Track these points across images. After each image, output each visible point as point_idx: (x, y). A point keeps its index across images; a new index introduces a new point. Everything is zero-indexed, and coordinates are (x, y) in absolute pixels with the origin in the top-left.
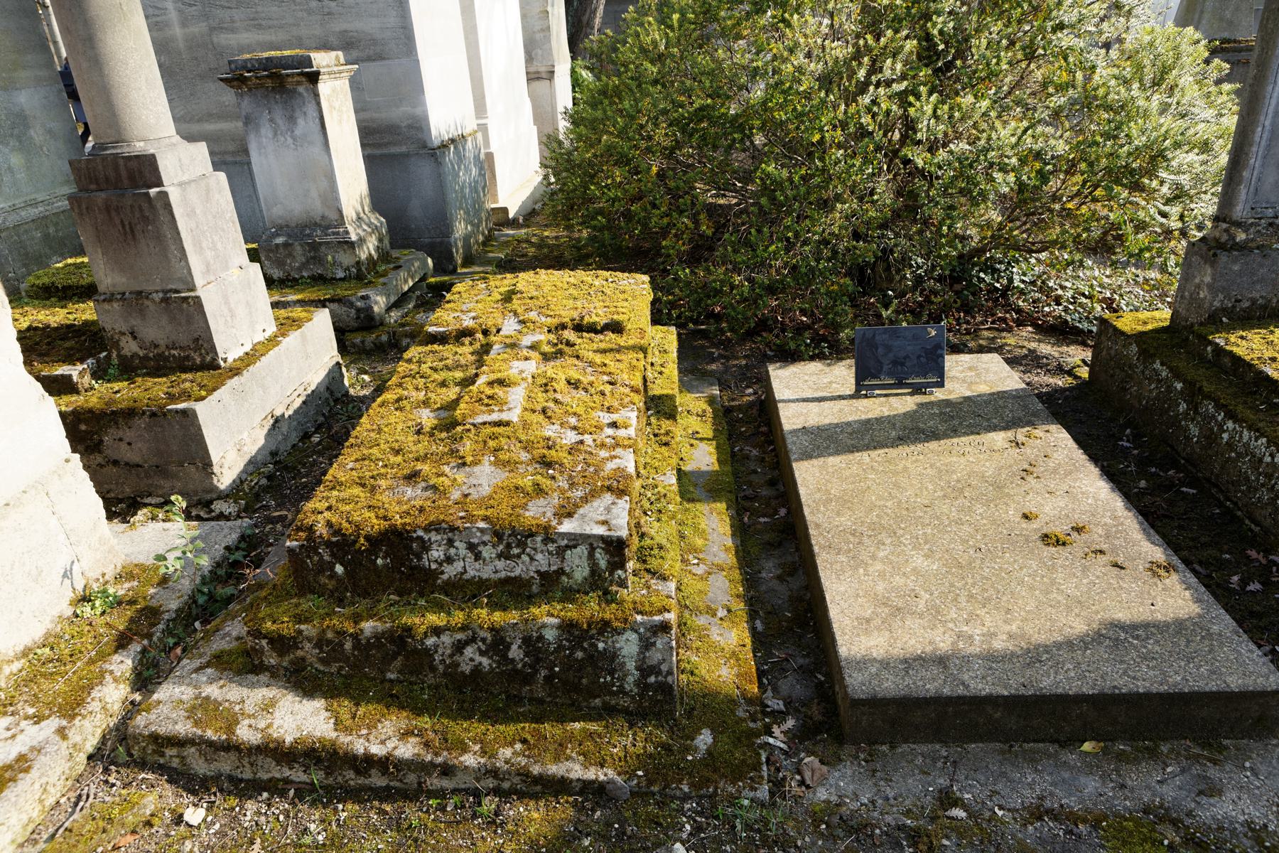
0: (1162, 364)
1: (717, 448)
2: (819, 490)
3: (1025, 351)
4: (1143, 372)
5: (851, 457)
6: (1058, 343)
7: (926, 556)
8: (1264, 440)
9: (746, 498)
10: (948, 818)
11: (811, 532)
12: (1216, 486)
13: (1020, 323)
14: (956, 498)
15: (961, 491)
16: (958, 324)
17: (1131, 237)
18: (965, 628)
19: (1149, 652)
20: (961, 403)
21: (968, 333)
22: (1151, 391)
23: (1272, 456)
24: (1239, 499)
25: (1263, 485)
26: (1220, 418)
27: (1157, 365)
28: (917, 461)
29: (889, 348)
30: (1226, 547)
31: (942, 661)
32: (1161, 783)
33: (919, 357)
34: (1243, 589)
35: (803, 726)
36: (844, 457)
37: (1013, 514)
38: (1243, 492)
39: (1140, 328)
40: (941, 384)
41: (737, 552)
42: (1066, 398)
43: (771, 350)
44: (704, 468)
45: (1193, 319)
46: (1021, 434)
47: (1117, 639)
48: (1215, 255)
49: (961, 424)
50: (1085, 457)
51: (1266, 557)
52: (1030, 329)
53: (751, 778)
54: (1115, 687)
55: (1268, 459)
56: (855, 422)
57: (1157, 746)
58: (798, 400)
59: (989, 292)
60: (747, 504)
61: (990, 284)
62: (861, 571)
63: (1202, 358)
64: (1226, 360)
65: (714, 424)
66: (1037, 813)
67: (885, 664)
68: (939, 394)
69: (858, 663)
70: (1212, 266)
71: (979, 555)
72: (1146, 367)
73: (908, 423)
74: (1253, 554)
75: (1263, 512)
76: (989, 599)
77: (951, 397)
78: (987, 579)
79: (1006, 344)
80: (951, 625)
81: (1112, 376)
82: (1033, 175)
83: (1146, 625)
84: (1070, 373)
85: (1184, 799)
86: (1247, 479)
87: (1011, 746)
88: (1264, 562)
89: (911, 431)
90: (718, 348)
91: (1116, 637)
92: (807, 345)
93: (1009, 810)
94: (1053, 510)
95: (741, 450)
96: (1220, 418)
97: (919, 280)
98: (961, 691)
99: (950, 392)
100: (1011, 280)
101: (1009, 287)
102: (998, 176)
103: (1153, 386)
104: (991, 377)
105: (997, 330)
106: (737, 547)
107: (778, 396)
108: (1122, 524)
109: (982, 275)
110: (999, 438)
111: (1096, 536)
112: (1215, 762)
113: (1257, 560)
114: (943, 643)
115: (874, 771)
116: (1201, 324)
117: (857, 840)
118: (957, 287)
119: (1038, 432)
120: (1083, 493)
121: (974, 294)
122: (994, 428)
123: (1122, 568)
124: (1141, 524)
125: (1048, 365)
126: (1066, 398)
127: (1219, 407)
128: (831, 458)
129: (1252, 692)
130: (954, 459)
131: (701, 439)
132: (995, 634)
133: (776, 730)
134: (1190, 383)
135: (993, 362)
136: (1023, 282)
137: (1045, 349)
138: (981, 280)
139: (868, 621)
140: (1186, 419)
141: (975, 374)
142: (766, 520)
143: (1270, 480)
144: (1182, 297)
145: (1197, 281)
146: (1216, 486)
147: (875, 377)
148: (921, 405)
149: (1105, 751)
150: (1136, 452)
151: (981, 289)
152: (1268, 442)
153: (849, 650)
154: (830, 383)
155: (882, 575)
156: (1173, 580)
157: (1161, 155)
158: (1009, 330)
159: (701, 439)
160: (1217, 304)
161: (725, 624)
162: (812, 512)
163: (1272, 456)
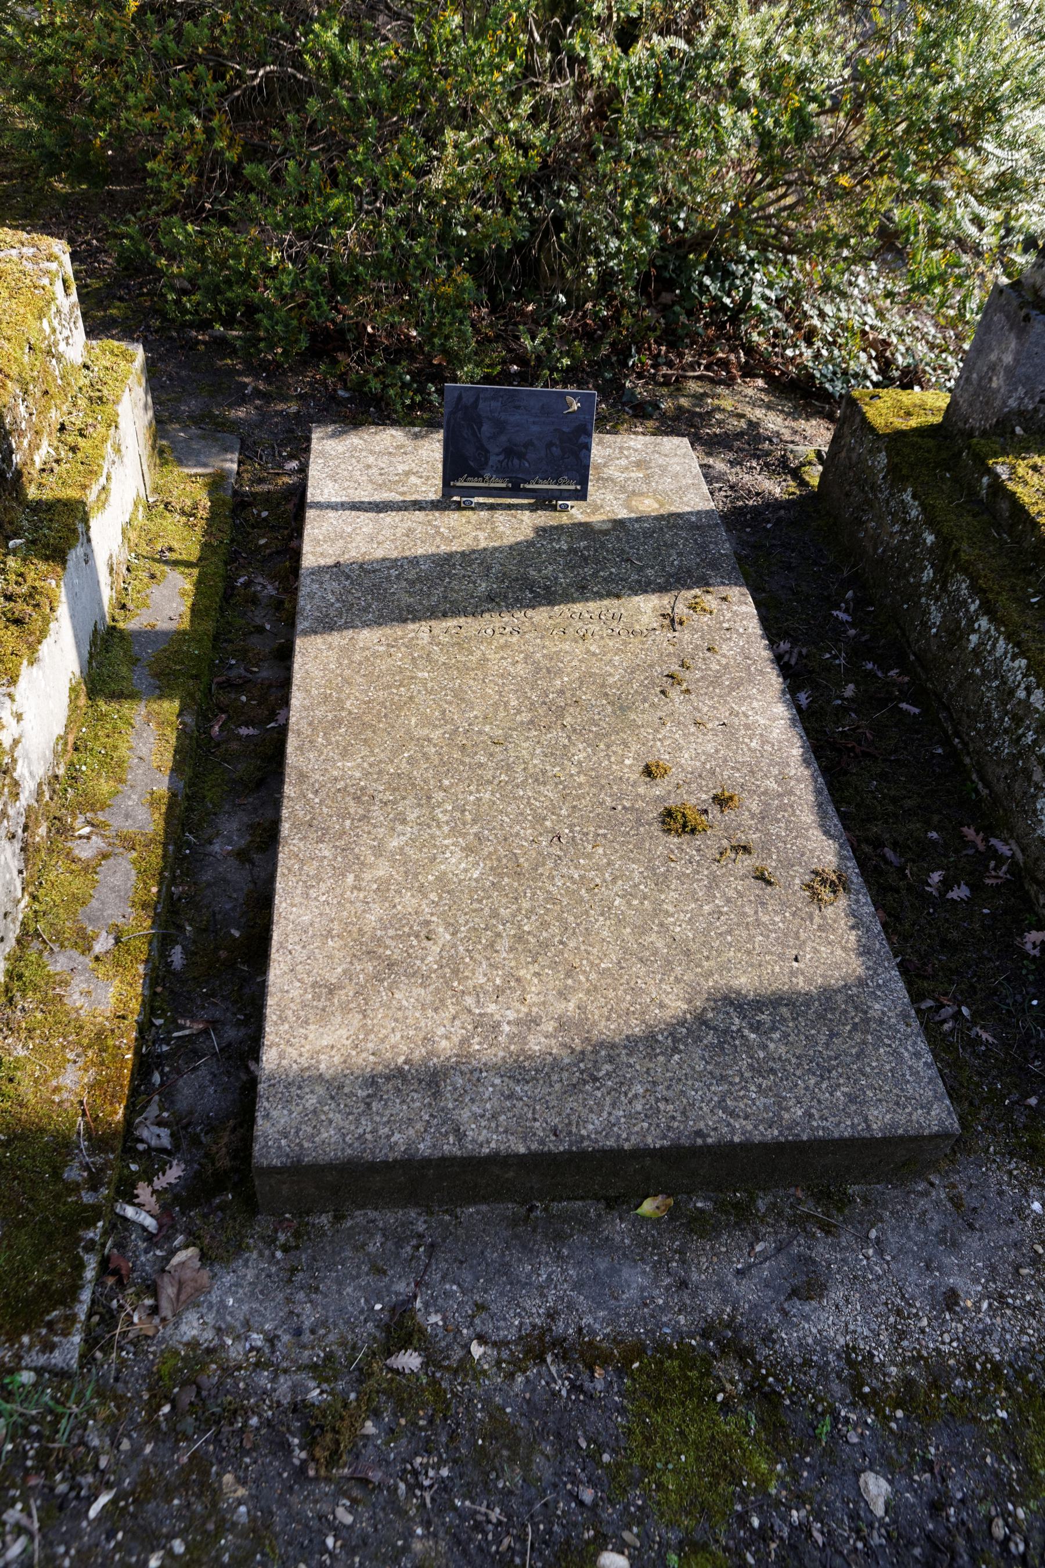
0: (914, 497)
1: (199, 583)
2: (326, 698)
3: (743, 424)
4: (888, 502)
5: (397, 631)
6: (794, 414)
7: (469, 850)
8: (1024, 662)
9: (228, 685)
10: (391, 1370)
11: (289, 790)
12: (947, 708)
13: (748, 372)
14: (548, 728)
15: (561, 712)
16: (655, 366)
17: (921, 255)
18: (492, 1008)
19: (770, 1057)
20: (606, 533)
21: (666, 383)
22: (892, 535)
23: (1029, 690)
24: (972, 739)
25: (1006, 731)
26: (973, 608)
27: (907, 497)
28: (503, 647)
29: (500, 426)
30: (936, 818)
31: (431, 1079)
32: (734, 1277)
33: (550, 444)
34: (942, 894)
35: (198, 1175)
36: (388, 631)
37: (630, 766)
38: (978, 732)
39: (901, 424)
40: (581, 495)
41: (170, 807)
42: (778, 522)
43: (345, 388)
44: (163, 625)
45: (975, 422)
46: (681, 601)
47: (726, 1031)
48: (1027, 318)
49: (595, 575)
50: (767, 654)
51: (986, 840)
52: (760, 382)
53: (50, 1325)
54: (699, 1133)
55: (1021, 694)
56: (427, 557)
57: (753, 1200)
58: (343, 506)
59: (713, 311)
60: (224, 699)
61: (716, 298)
62: (350, 879)
63: (972, 492)
64: (1004, 505)
65: (206, 533)
66: (537, 1346)
67: (334, 1088)
68: (577, 513)
69: (289, 1085)
70: (1019, 337)
71: (556, 851)
72: (892, 495)
73: (512, 568)
74: (969, 832)
75: (998, 770)
76: (545, 945)
77: (596, 518)
78: (554, 901)
79: (718, 409)
80: (469, 1001)
81: (847, 495)
82: (784, 119)
83: (775, 1002)
84: (796, 474)
85: (767, 1307)
86: (988, 714)
87: (531, 1209)
88: (982, 847)
89: (516, 584)
90: (257, 377)
91: (729, 1023)
92: (404, 385)
93: (495, 1344)
94: (691, 755)
95: (247, 585)
96: (973, 608)
97: (607, 278)
98: (449, 1147)
99: (596, 508)
100: (748, 294)
101: (743, 305)
102: (726, 112)
103: (896, 528)
104: (667, 483)
105: (711, 380)
106: (174, 795)
107: (310, 498)
108: (791, 793)
109: (707, 280)
110: (647, 606)
111: (742, 822)
112: (828, 1229)
113: (974, 845)
114: (445, 1037)
115: (293, 1270)
116: (984, 434)
117: (216, 1440)
118: (666, 297)
119: (710, 601)
120: (747, 727)
121: (690, 313)
122: (643, 587)
123: (769, 883)
124: (818, 792)
125: (768, 453)
126: (778, 522)
127: (976, 590)
128: (366, 633)
129: (901, 1138)
130: (566, 646)
131: (176, 563)
132: (536, 1021)
133: (143, 1192)
134: (945, 539)
135: (678, 454)
136: (765, 299)
137: (773, 422)
138: (704, 289)
139: (332, 990)
140: (928, 595)
141: (646, 474)
142: (251, 731)
143: (1018, 727)
144: (968, 379)
145: (993, 357)
146: (947, 708)
147: (476, 474)
148: (542, 532)
149: (674, 1213)
150: (852, 632)
151: (702, 306)
152: (1029, 667)
153: (281, 1056)
154: (407, 474)
155: (383, 888)
156: (837, 909)
157: (993, 107)
158: (729, 382)
159: (176, 563)
160: (1012, 403)
161: (102, 970)
162: (300, 748)
163: (1029, 690)
